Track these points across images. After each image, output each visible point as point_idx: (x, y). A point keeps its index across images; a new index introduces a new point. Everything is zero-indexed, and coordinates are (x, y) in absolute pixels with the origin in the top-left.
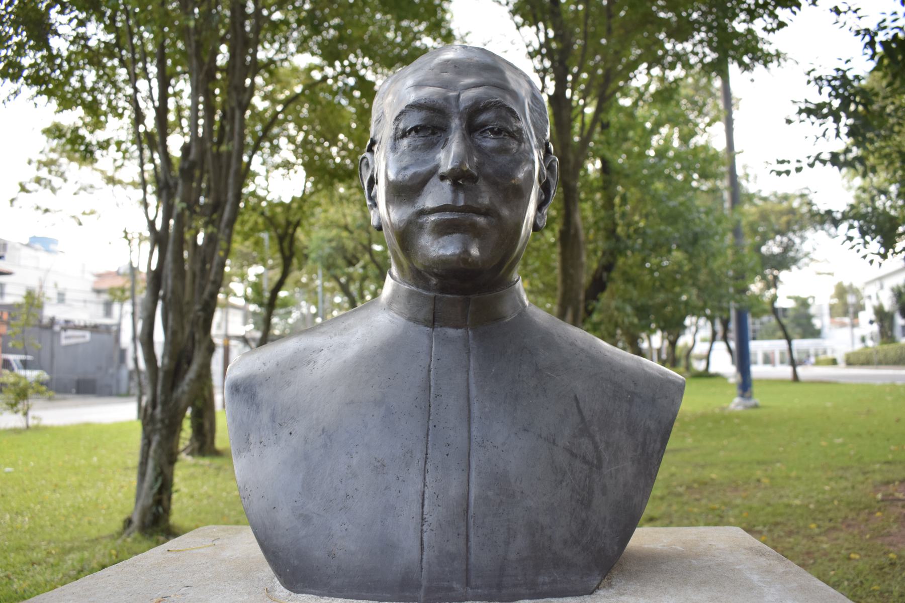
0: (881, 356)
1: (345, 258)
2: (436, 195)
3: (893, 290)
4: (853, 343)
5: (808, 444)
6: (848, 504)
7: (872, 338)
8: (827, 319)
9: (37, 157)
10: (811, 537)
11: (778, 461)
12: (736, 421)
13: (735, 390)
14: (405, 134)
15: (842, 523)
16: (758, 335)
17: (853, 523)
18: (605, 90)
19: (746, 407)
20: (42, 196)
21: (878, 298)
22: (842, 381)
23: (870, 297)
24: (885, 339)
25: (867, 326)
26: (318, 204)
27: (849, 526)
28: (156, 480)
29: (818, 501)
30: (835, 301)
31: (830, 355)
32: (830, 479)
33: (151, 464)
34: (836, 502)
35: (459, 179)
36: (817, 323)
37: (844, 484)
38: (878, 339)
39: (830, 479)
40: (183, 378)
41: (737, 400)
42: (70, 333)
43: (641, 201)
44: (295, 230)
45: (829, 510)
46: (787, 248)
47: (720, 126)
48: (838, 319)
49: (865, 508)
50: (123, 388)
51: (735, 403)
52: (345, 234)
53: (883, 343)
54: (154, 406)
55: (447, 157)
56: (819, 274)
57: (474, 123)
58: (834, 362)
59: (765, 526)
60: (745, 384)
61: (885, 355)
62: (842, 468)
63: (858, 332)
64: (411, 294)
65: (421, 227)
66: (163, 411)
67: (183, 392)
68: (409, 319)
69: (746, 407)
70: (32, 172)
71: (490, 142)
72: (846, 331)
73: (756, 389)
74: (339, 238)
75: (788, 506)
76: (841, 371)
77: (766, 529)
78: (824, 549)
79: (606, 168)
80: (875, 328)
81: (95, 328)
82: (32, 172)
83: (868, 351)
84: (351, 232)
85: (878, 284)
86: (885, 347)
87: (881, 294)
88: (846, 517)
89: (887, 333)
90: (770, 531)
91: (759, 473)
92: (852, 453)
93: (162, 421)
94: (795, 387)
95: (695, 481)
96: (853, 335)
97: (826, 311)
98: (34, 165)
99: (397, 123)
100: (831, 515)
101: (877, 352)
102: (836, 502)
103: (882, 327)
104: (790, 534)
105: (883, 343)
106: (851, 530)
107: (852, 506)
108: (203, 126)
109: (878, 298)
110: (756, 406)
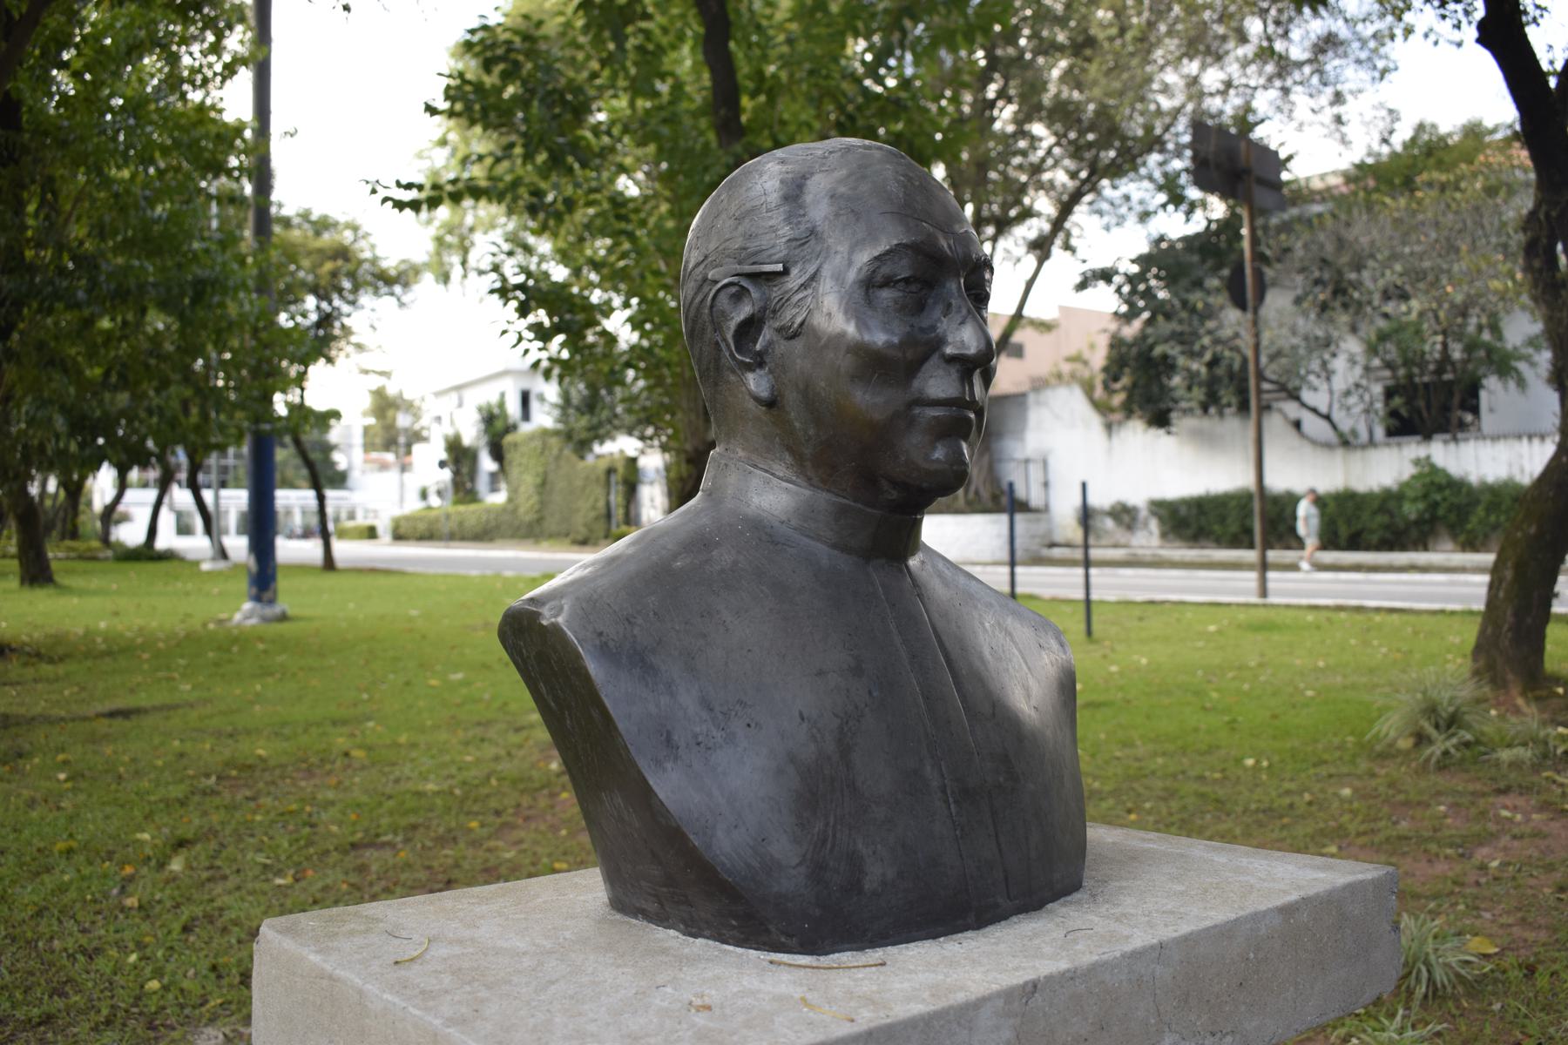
0: (452, 525)
3: (480, 409)
4: (402, 500)
5: (408, 683)
6: (514, 782)
7: (440, 493)
8: (358, 454)
10: (476, 844)
11: (369, 719)
12: (261, 646)
13: (243, 585)
14: (888, 282)
15: (516, 814)
16: (230, 477)
17: (531, 812)
19: (265, 619)
21: (452, 422)
22: (410, 569)
23: (438, 419)
24: (461, 494)
25: (429, 465)
27: (527, 819)
29: (464, 783)
30: (372, 421)
31: (361, 521)
32: (467, 743)
34: (494, 782)
36: (340, 460)
37: (490, 751)
38: (450, 494)
39: (467, 743)
41: (248, 606)
45: (488, 796)
46: (326, 320)
47: (245, 76)
48: (374, 455)
49: (543, 787)
51: (244, 612)
53: (457, 502)
56: (366, 372)
58: (371, 533)
59: (395, 833)
60: (264, 575)
61: (461, 524)
62: (479, 724)
63: (414, 481)
64: (842, 511)
65: (911, 422)
68: (834, 546)
69: (265, 619)
72: (393, 476)
73: (283, 583)
75: (419, 794)
76: (383, 550)
77: (399, 839)
78: (509, 861)
80: (446, 475)
83: (433, 514)
85: (454, 396)
86: (461, 508)
87: (458, 414)
88: (518, 805)
89: (463, 484)
90: (407, 840)
91: (341, 742)
92: (487, 696)
94: (330, 580)
95: (228, 764)
96: (402, 485)
97: (358, 439)
99: (877, 264)
100: (493, 803)
101: (448, 516)
102: (494, 782)
103: (456, 473)
104: (441, 841)
105: (457, 502)
106: (533, 825)
107: (521, 786)
109: (452, 422)
110: (283, 618)
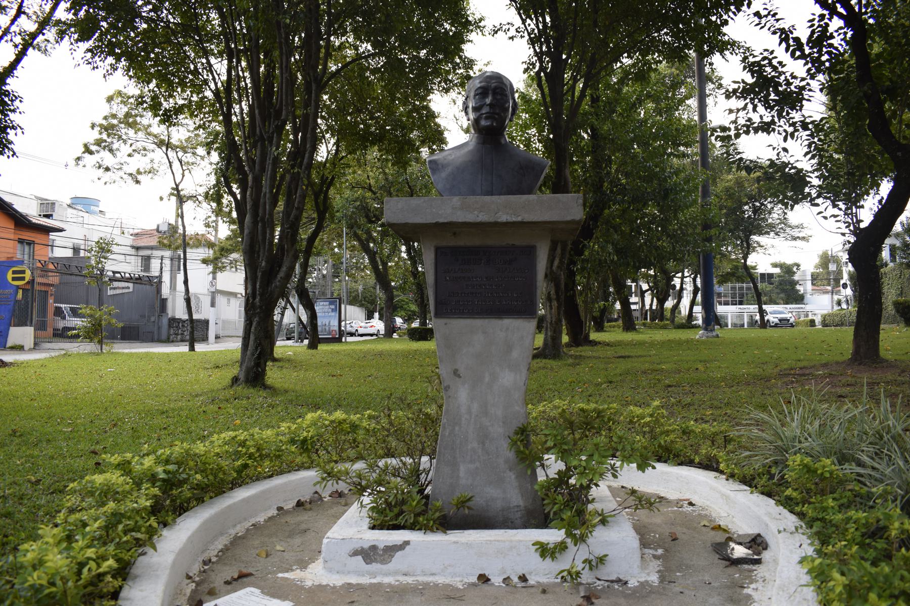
1: (367, 216)
2: (485, 110)
9: (100, 120)
18: (594, 70)
20: (106, 157)
26: (349, 166)
28: (256, 348)
33: (252, 337)
35: (491, 105)
40: (276, 276)
42: (116, 284)
43: (624, 163)
44: (328, 188)
50: (164, 336)
52: (369, 194)
54: (254, 298)
55: (488, 101)
57: (495, 93)
66: (261, 300)
67: (276, 286)
70: (95, 135)
71: (499, 97)
74: (364, 198)
79: (594, 136)
81: (137, 280)
82: (95, 135)
84: (374, 193)
93: (261, 307)
98: (97, 129)
108: (252, 94)
